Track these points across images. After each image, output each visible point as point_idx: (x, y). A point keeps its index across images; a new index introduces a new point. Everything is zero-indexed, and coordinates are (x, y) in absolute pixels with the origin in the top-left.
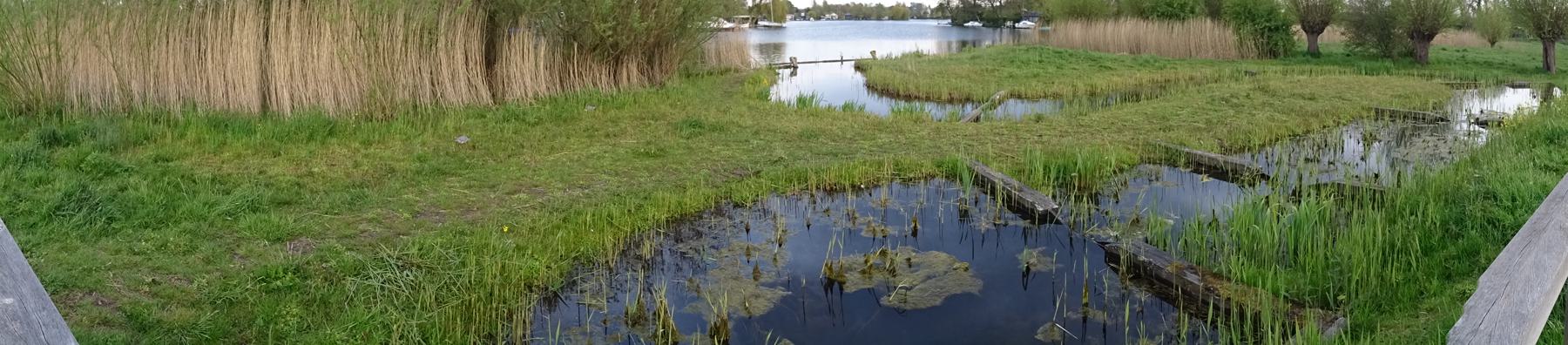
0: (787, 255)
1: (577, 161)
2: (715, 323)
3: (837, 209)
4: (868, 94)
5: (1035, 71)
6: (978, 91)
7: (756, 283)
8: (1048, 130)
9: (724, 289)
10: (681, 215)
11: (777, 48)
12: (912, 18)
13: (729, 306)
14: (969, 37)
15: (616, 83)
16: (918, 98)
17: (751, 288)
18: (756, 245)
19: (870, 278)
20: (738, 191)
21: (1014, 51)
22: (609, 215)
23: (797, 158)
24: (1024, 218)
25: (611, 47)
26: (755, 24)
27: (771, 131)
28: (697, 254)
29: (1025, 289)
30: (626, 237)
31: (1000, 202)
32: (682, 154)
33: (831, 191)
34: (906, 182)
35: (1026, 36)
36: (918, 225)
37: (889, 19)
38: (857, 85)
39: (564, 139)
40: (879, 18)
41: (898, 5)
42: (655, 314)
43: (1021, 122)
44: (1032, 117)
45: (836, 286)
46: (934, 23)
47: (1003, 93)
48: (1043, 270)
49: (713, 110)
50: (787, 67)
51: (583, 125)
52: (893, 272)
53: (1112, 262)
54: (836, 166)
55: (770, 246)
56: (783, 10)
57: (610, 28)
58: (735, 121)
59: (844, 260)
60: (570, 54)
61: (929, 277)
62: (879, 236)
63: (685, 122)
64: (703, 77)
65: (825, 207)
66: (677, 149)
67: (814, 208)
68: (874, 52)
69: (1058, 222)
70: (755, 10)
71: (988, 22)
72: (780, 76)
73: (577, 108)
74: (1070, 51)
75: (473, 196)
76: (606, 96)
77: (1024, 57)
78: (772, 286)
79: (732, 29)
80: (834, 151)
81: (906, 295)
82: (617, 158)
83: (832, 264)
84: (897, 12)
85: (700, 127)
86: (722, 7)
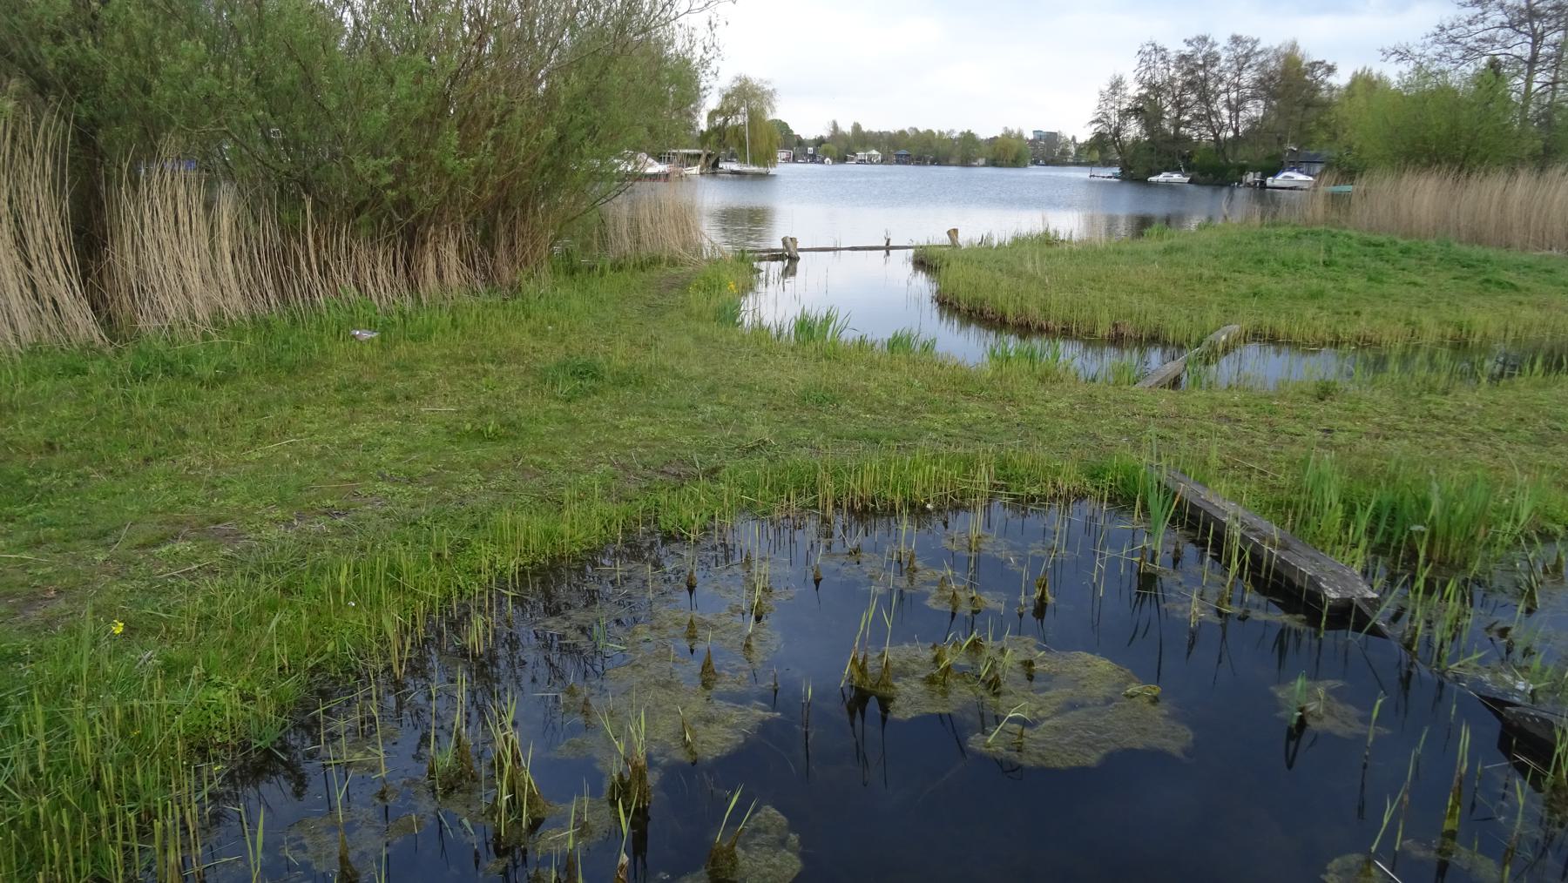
0: (771, 640)
1: (318, 457)
2: (621, 775)
3: (877, 549)
4: (941, 318)
5: (1314, 284)
6: (1177, 323)
7: (708, 693)
8: (1346, 419)
9: (639, 707)
10: (553, 559)
11: (756, 218)
12: (1036, 163)
13: (650, 740)
14: (1157, 206)
15: (413, 286)
16: (1042, 330)
17: (697, 705)
18: (708, 618)
19: (945, 694)
20: (673, 508)
21: (1264, 238)
22: (391, 568)
23: (793, 444)
24: (1287, 608)
25: (397, 210)
26: (713, 168)
27: (743, 387)
28: (585, 639)
29: (1290, 766)
30: (431, 611)
31: (1235, 565)
32: (554, 434)
33: (865, 513)
34: (1021, 503)
35: (1291, 207)
36: (1047, 595)
37: (986, 165)
38: (918, 300)
39: (288, 411)
40: (966, 162)
41: (1008, 135)
42: (493, 765)
43: (1282, 397)
44: (1311, 390)
45: (873, 705)
46: (1082, 174)
47: (1235, 328)
48: (1338, 732)
49: (621, 347)
50: (776, 258)
51: (333, 377)
52: (994, 685)
53: (1523, 754)
54: (876, 462)
55: (738, 620)
56: (771, 139)
57: (389, 169)
58: (668, 364)
59: (893, 653)
60: (296, 222)
61: (1072, 706)
62: (965, 609)
63: (562, 366)
64: (602, 274)
65: (851, 544)
66: (546, 424)
67: (829, 548)
68: (955, 231)
69: (1376, 631)
70: (713, 138)
71: (1203, 172)
72: (762, 275)
73: (320, 340)
74: (1402, 242)
75: (46, 564)
76: (388, 313)
77: (1290, 252)
78: (739, 699)
79: (666, 177)
80: (872, 432)
81: (1021, 736)
82: (411, 445)
83: (865, 658)
84: (1005, 150)
85: (593, 376)
86: (645, 130)
